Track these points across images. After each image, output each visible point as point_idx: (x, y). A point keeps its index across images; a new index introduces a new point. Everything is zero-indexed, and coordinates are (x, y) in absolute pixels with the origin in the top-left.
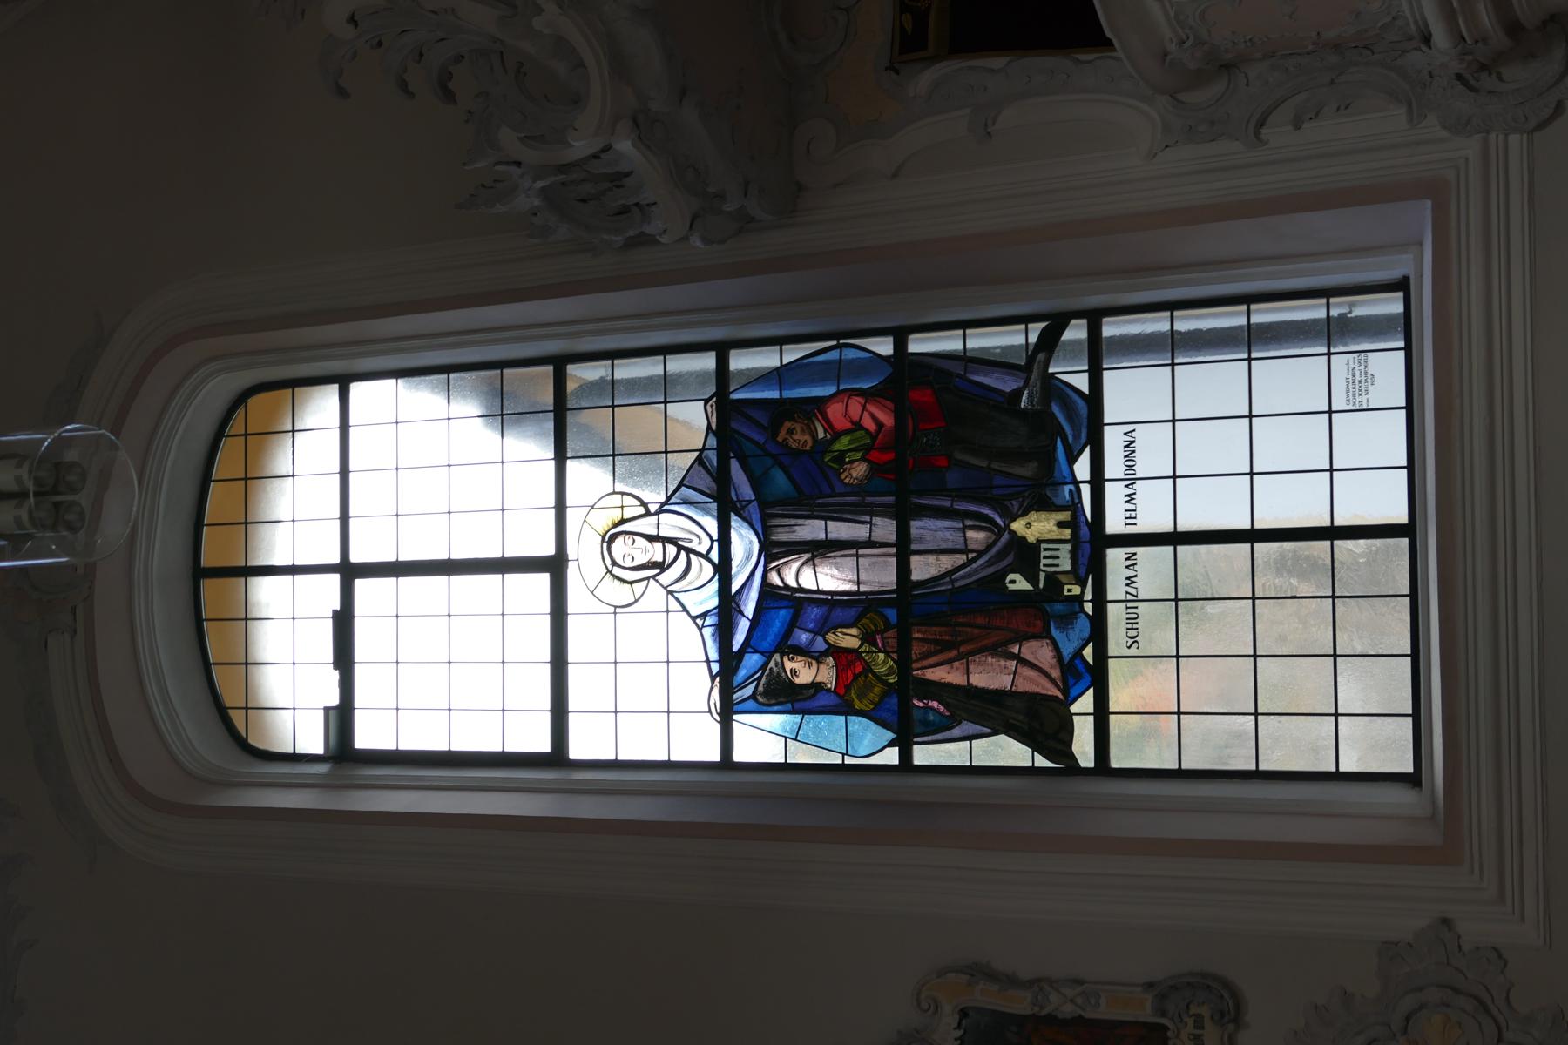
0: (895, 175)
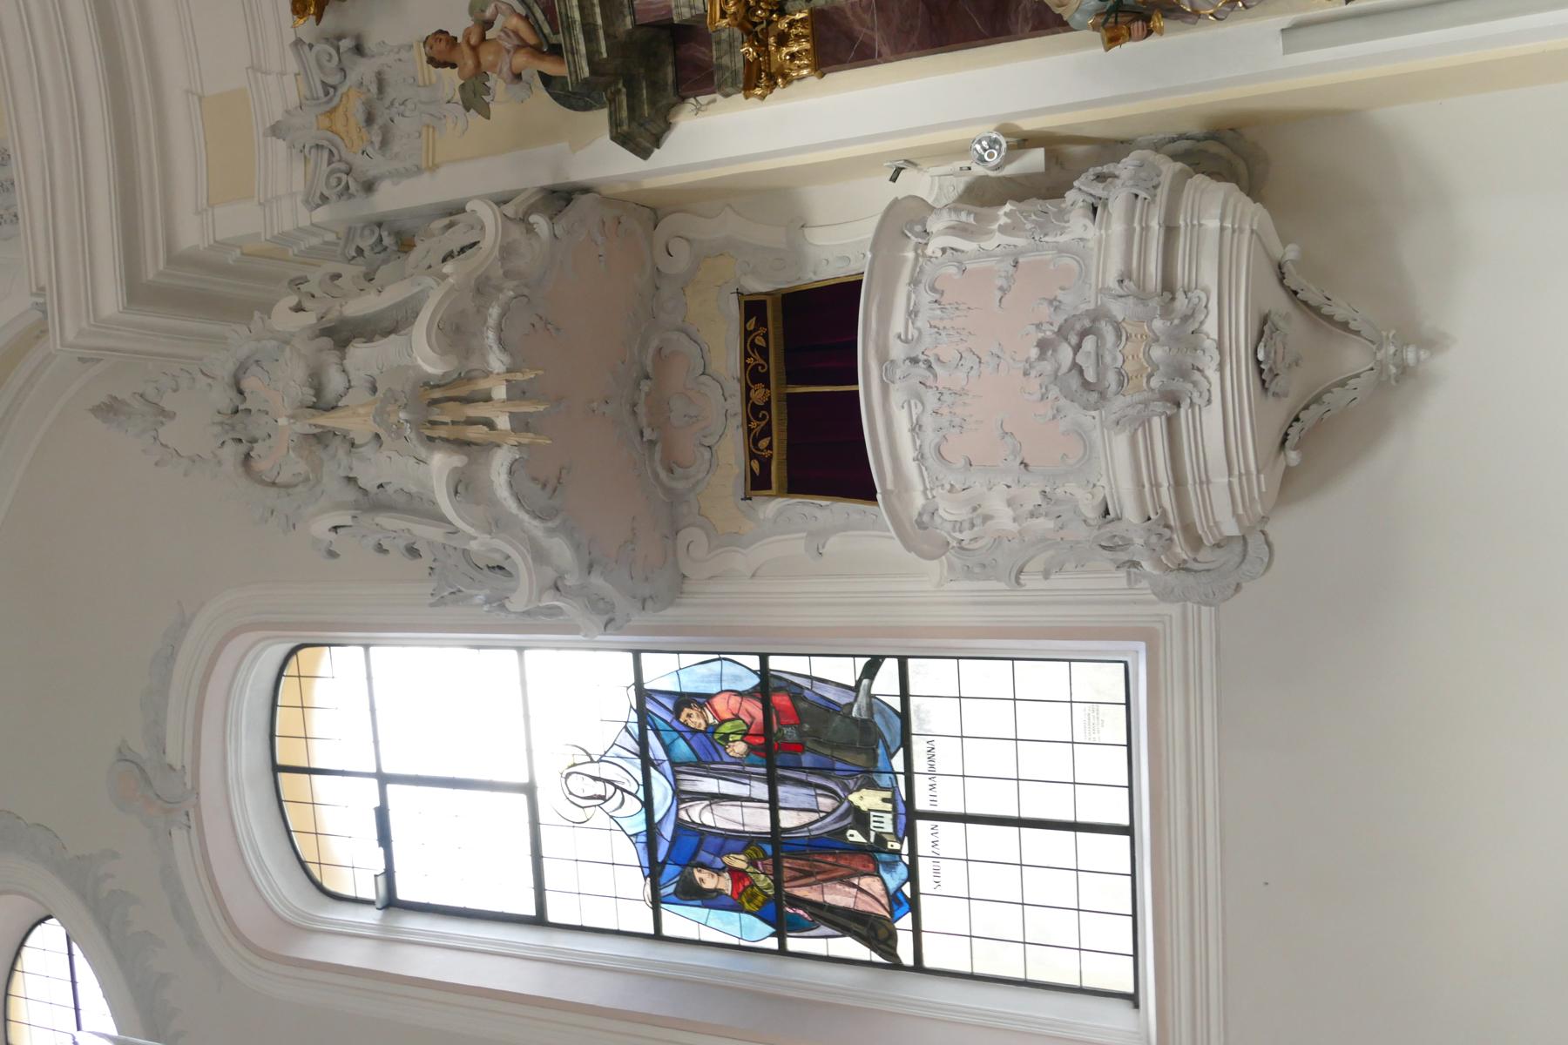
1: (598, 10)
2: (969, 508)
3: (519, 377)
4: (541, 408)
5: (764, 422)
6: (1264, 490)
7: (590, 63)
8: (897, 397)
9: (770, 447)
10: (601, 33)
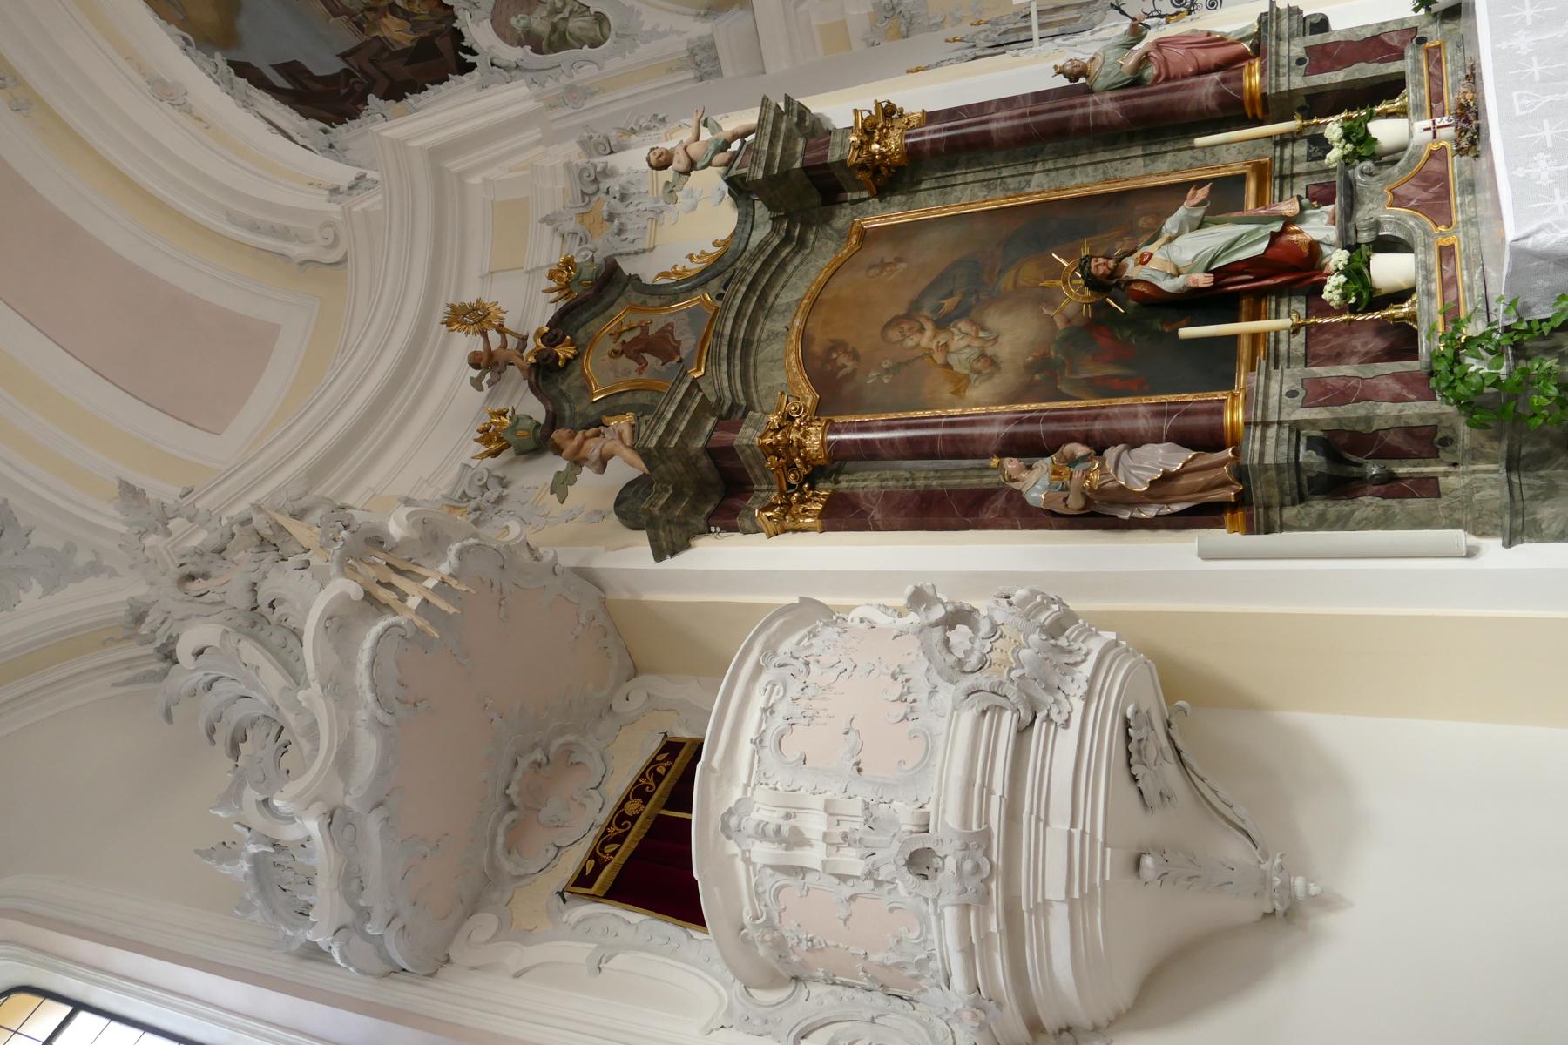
0: (517, 975)
1: (685, 423)
2: (782, 812)
3: (454, 583)
4: (452, 610)
5: (621, 831)
6: (1108, 878)
7: (659, 441)
8: (765, 678)
9: (614, 853)
10: (678, 435)
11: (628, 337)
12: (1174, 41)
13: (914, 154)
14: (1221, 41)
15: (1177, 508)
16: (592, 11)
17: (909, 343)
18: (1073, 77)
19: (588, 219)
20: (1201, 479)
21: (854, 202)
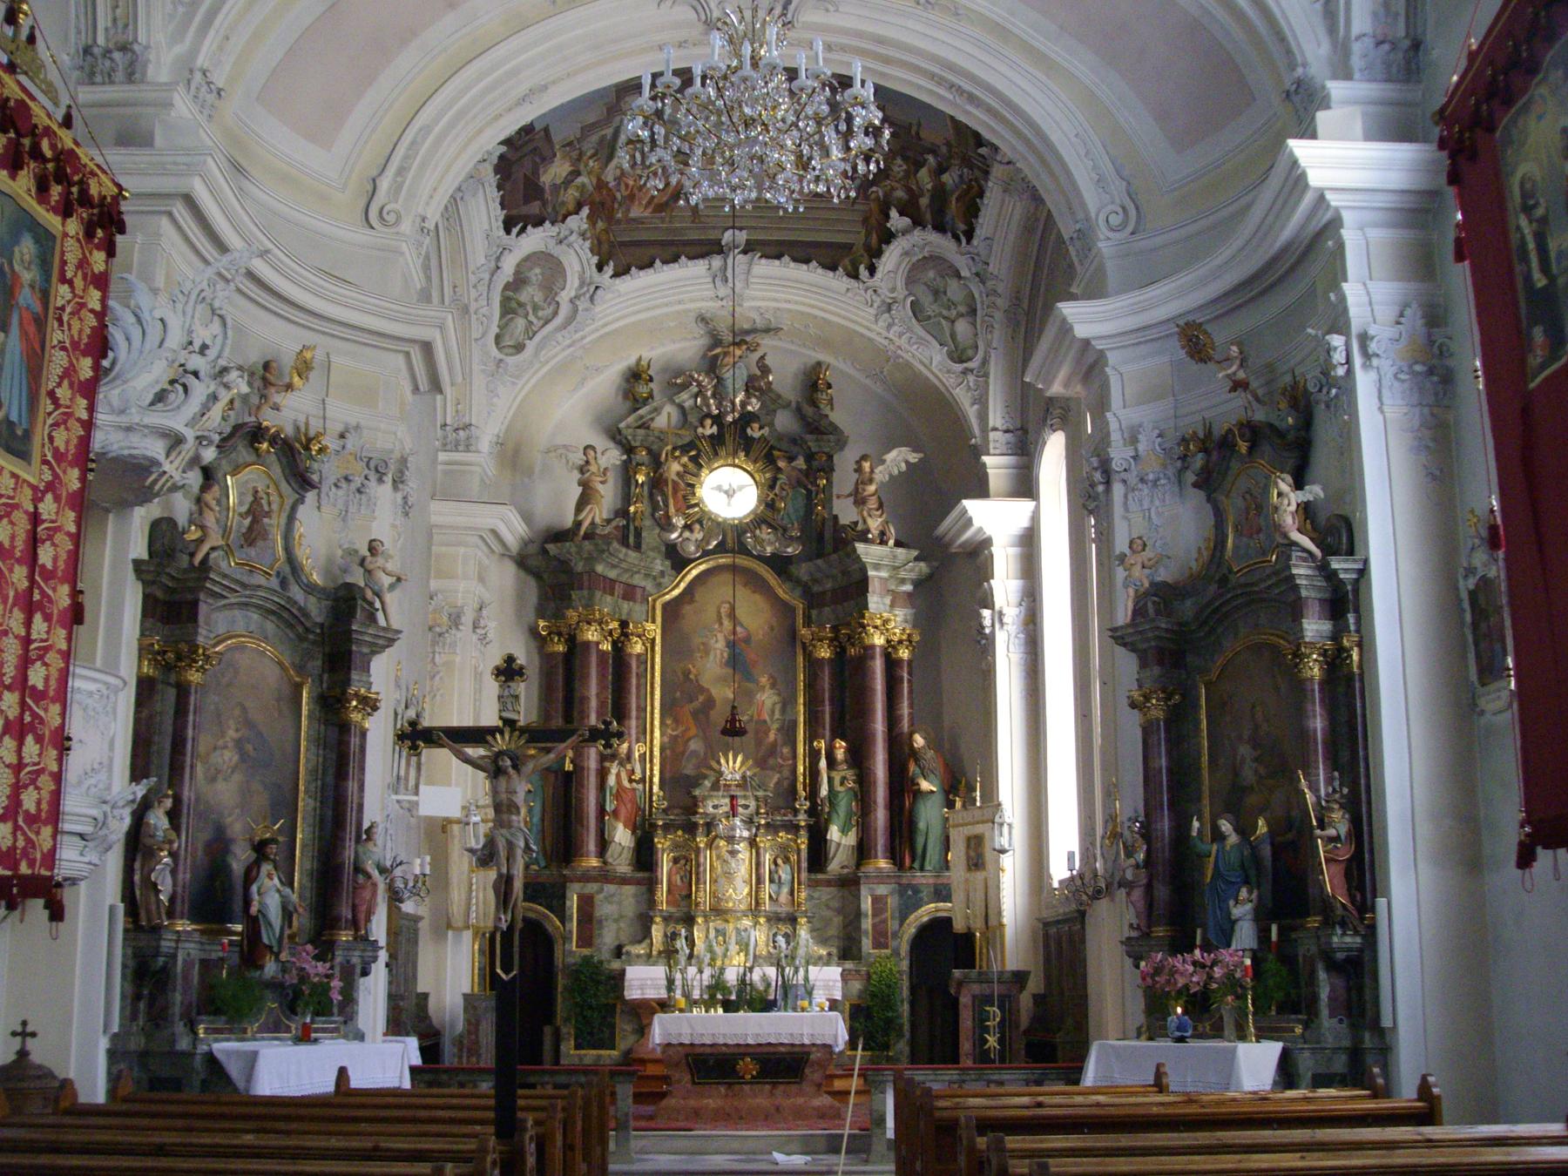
11: (264, 502)
12: (374, 894)
13: (344, 728)
14: (368, 920)
15: (138, 893)
16: (527, 342)
17: (231, 722)
18: (368, 831)
19: (351, 458)
20: (154, 907)
21: (321, 676)
